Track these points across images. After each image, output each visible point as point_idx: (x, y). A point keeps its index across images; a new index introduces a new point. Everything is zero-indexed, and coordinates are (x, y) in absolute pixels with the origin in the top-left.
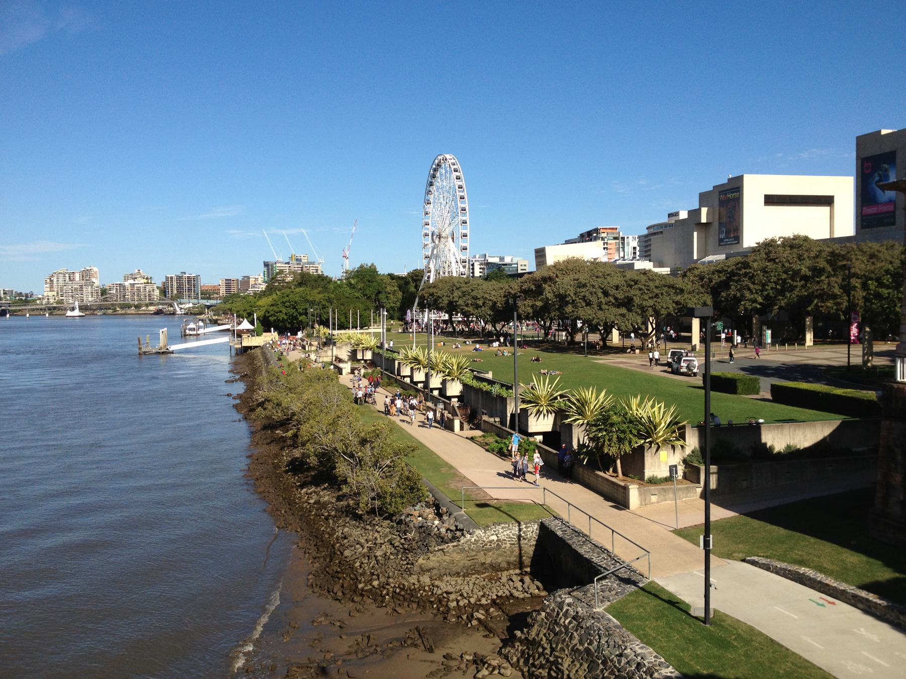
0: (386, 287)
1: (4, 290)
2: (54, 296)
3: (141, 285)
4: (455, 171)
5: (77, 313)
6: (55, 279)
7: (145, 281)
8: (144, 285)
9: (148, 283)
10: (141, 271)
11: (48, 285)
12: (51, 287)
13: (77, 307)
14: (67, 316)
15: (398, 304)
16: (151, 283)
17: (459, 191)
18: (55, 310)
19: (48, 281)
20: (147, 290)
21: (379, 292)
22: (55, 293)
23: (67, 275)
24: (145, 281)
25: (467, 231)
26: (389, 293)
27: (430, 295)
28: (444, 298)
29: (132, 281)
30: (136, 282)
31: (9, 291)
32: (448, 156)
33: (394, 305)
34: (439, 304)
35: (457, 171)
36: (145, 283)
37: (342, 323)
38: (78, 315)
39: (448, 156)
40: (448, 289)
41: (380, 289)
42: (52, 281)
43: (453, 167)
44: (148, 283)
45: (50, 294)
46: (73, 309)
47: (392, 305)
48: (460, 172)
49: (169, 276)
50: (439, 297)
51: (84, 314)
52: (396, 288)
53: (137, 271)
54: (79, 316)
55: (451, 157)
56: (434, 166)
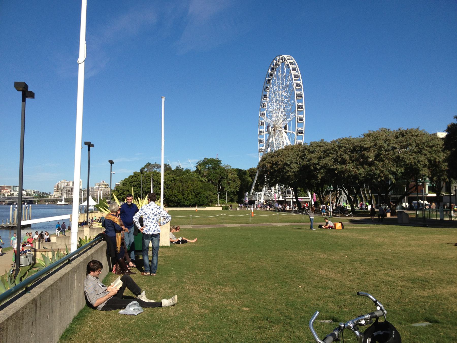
0: (228, 175)
1: (34, 191)
2: (58, 194)
3: (102, 189)
4: (293, 70)
5: (63, 203)
6: (60, 185)
7: (105, 186)
8: (103, 188)
9: (106, 187)
10: (104, 181)
11: (56, 189)
12: (57, 189)
13: (64, 199)
14: (58, 205)
15: (238, 189)
16: (107, 187)
17: (297, 90)
18: (55, 201)
19: (56, 186)
20: (105, 191)
21: (222, 178)
22: (59, 193)
23: (66, 183)
24: (105, 186)
25: (303, 116)
26: (230, 180)
27: (273, 164)
28: (294, 165)
29: (97, 186)
30: (100, 187)
31: (36, 191)
32: (286, 57)
33: (234, 190)
34: (286, 172)
35: (295, 70)
36: (104, 187)
37: (179, 200)
38: (64, 204)
39: (286, 57)
40: (298, 155)
41: (223, 176)
42: (58, 186)
43: (291, 67)
44: (106, 187)
45: (57, 193)
46: (61, 201)
47: (233, 189)
48: (297, 72)
49: (117, 184)
50: (286, 164)
51: (67, 204)
52: (236, 176)
53: (102, 181)
54: (64, 205)
55: (288, 58)
56: (272, 66)
